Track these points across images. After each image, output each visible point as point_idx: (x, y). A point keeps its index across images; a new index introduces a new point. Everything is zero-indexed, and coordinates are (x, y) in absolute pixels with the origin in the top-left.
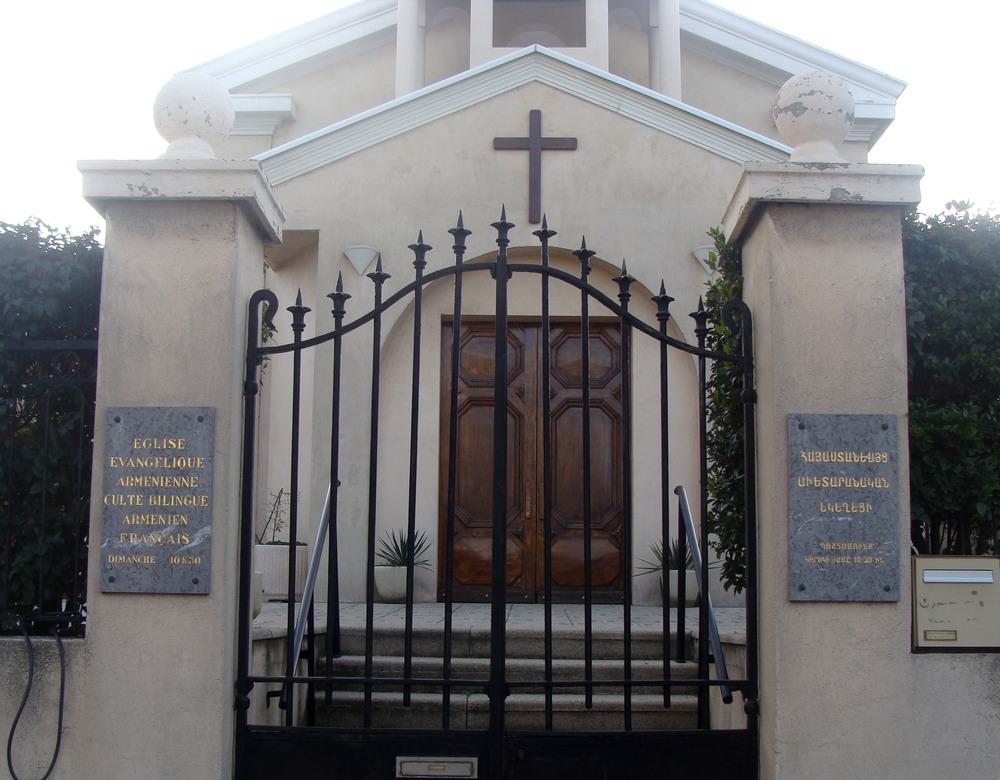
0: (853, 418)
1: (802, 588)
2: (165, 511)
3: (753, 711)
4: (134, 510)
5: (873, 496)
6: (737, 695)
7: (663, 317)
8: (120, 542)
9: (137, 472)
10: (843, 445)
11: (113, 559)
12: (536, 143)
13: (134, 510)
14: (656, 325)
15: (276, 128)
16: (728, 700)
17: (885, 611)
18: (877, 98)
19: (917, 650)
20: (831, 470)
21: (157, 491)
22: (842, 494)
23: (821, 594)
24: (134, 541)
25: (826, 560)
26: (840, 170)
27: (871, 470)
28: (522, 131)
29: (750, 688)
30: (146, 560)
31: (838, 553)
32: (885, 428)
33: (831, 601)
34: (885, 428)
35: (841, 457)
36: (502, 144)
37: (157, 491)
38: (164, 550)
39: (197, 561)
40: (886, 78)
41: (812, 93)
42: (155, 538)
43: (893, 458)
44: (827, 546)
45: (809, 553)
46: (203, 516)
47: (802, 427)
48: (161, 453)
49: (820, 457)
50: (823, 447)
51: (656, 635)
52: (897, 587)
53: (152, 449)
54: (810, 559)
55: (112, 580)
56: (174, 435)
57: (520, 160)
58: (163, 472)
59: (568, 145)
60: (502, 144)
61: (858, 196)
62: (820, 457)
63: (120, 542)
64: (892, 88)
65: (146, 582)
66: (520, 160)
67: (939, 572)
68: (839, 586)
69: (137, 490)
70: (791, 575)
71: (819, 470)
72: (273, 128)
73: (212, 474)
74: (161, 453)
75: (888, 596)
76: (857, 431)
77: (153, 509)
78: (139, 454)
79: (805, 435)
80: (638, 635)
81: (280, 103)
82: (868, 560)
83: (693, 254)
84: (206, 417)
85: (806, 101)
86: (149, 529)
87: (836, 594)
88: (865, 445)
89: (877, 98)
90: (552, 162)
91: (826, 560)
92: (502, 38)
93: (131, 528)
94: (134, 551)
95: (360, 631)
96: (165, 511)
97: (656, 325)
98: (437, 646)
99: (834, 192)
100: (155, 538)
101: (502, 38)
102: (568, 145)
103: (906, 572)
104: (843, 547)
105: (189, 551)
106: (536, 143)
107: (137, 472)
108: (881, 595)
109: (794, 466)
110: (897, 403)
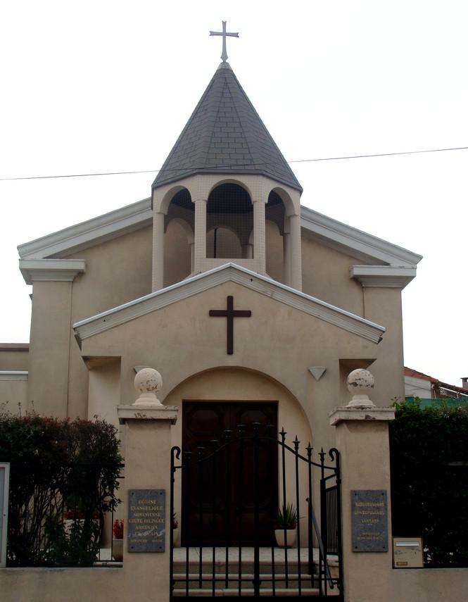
0: (373, 491)
1: (356, 547)
2: (150, 524)
3: (341, 588)
4: (139, 524)
5: (379, 517)
6: (335, 586)
7: (310, 454)
8: (135, 535)
9: (140, 511)
10: (369, 500)
11: (132, 541)
12: (230, 313)
13: (139, 524)
14: (307, 457)
15: (75, 278)
16: (332, 587)
17: (383, 555)
18: (406, 265)
19: (394, 568)
20: (366, 509)
21: (147, 518)
22: (369, 516)
23: (362, 549)
24: (140, 535)
25: (364, 538)
26: (368, 409)
27: (378, 509)
28: (222, 306)
29: (340, 582)
30: (144, 541)
31: (368, 536)
32: (383, 494)
33: (366, 552)
34: (383, 494)
35: (368, 504)
36: (213, 314)
37: (147, 518)
38: (150, 538)
39: (161, 541)
40: (411, 253)
41: (360, 379)
42: (146, 534)
43: (386, 505)
44: (364, 534)
45: (358, 536)
46: (162, 526)
47: (356, 495)
48: (148, 505)
49: (361, 504)
50: (362, 501)
51: (295, 563)
52: (387, 547)
53: (145, 504)
54: (359, 538)
55: (132, 548)
56: (153, 500)
57: (222, 322)
58: (149, 511)
59: (247, 314)
60: (213, 314)
61: (374, 418)
62: (361, 504)
63: (135, 535)
64: (416, 259)
65: (144, 548)
66: (222, 322)
67: (402, 543)
68: (368, 547)
69: (140, 517)
70: (353, 543)
71: (361, 509)
72: (73, 277)
73: (165, 512)
74: (148, 505)
75: (385, 550)
76: (376, 495)
77: (146, 524)
78: (141, 505)
79: (357, 497)
80: (231, 562)
81: (78, 264)
82: (377, 538)
83: (309, 370)
84: (162, 492)
85: (358, 382)
86: (144, 531)
87: (368, 549)
88: (377, 500)
89: (406, 265)
90: (239, 323)
91: (364, 538)
92: (214, 251)
93: (138, 530)
94: (140, 537)
95: (184, 563)
96: (150, 524)
97: (307, 457)
98: (223, 569)
99: (367, 416)
100: (146, 534)
101: (214, 251)
102: (247, 314)
103: (390, 542)
104: (369, 534)
105: (158, 538)
106: (230, 313)
107: (140, 511)
108: (383, 549)
109: (353, 507)
110: (387, 487)
